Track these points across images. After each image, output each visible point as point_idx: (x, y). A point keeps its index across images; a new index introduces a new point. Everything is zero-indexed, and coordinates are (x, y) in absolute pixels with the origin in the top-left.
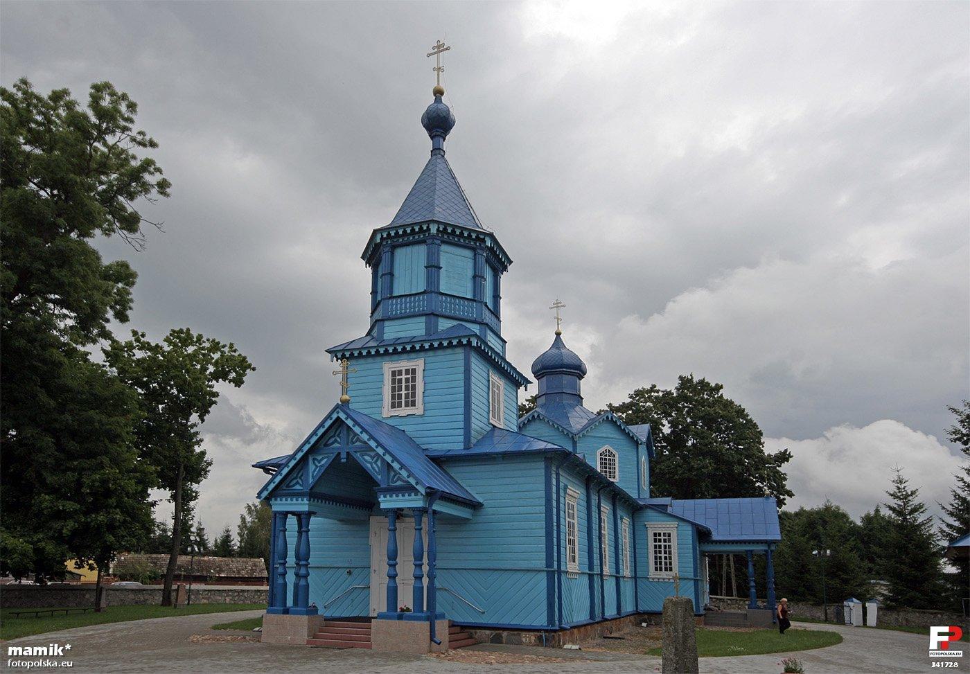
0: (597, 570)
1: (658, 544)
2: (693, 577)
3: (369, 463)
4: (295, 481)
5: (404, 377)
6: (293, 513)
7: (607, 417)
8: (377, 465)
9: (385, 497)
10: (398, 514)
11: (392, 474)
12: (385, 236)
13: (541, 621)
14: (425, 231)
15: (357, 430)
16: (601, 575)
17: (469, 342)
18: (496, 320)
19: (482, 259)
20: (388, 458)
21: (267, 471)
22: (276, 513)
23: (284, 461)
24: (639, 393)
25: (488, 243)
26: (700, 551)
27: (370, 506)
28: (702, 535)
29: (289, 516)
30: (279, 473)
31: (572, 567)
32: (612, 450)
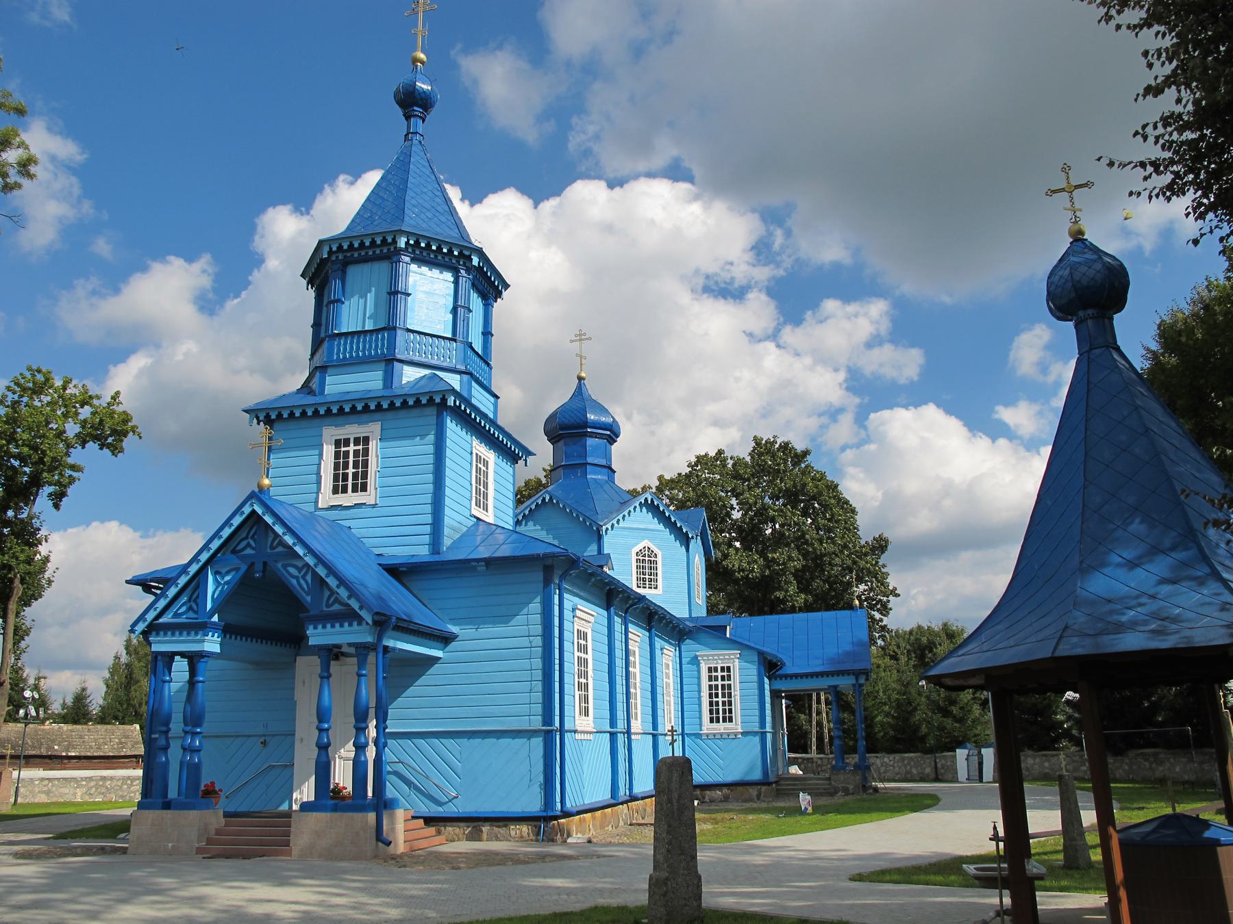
0: (621, 725)
1: (713, 683)
2: (757, 729)
3: (297, 578)
4: (243, 544)
5: (352, 448)
6: (183, 654)
7: (646, 499)
8: (306, 582)
9: (315, 628)
10: (332, 653)
11: (327, 593)
12: (334, 249)
13: (534, 805)
14: (390, 244)
15: (279, 529)
16: (628, 732)
17: (444, 400)
18: (486, 368)
19: (465, 282)
20: (321, 571)
21: (147, 589)
22: (157, 655)
23: (174, 574)
24: (701, 460)
25: (475, 261)
26: (771, 691)
27: (296, 641)
28: (770, 667)
29: (177, 658)
30: (163, 595)
31: (584, 723)
32: (653, 548)
